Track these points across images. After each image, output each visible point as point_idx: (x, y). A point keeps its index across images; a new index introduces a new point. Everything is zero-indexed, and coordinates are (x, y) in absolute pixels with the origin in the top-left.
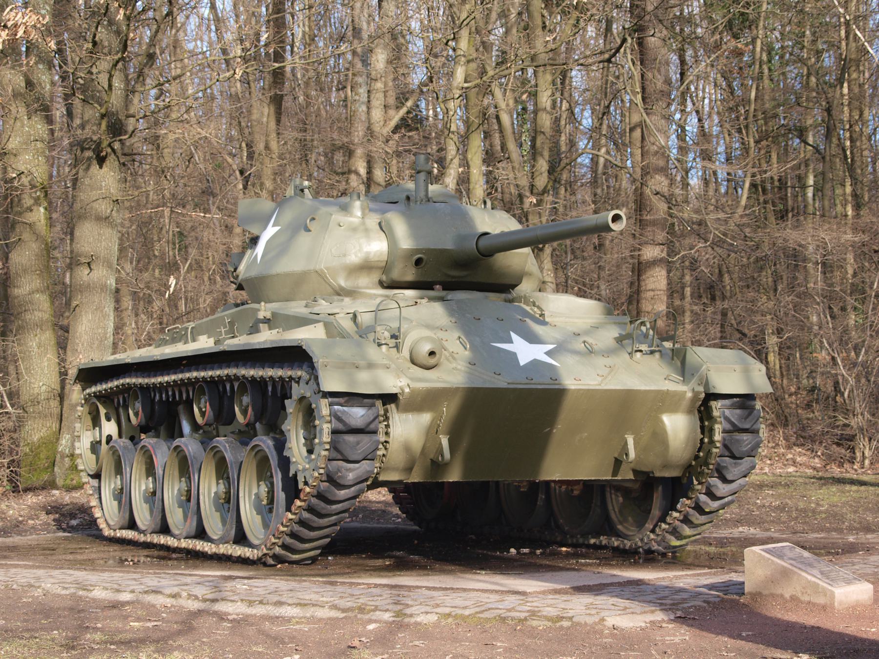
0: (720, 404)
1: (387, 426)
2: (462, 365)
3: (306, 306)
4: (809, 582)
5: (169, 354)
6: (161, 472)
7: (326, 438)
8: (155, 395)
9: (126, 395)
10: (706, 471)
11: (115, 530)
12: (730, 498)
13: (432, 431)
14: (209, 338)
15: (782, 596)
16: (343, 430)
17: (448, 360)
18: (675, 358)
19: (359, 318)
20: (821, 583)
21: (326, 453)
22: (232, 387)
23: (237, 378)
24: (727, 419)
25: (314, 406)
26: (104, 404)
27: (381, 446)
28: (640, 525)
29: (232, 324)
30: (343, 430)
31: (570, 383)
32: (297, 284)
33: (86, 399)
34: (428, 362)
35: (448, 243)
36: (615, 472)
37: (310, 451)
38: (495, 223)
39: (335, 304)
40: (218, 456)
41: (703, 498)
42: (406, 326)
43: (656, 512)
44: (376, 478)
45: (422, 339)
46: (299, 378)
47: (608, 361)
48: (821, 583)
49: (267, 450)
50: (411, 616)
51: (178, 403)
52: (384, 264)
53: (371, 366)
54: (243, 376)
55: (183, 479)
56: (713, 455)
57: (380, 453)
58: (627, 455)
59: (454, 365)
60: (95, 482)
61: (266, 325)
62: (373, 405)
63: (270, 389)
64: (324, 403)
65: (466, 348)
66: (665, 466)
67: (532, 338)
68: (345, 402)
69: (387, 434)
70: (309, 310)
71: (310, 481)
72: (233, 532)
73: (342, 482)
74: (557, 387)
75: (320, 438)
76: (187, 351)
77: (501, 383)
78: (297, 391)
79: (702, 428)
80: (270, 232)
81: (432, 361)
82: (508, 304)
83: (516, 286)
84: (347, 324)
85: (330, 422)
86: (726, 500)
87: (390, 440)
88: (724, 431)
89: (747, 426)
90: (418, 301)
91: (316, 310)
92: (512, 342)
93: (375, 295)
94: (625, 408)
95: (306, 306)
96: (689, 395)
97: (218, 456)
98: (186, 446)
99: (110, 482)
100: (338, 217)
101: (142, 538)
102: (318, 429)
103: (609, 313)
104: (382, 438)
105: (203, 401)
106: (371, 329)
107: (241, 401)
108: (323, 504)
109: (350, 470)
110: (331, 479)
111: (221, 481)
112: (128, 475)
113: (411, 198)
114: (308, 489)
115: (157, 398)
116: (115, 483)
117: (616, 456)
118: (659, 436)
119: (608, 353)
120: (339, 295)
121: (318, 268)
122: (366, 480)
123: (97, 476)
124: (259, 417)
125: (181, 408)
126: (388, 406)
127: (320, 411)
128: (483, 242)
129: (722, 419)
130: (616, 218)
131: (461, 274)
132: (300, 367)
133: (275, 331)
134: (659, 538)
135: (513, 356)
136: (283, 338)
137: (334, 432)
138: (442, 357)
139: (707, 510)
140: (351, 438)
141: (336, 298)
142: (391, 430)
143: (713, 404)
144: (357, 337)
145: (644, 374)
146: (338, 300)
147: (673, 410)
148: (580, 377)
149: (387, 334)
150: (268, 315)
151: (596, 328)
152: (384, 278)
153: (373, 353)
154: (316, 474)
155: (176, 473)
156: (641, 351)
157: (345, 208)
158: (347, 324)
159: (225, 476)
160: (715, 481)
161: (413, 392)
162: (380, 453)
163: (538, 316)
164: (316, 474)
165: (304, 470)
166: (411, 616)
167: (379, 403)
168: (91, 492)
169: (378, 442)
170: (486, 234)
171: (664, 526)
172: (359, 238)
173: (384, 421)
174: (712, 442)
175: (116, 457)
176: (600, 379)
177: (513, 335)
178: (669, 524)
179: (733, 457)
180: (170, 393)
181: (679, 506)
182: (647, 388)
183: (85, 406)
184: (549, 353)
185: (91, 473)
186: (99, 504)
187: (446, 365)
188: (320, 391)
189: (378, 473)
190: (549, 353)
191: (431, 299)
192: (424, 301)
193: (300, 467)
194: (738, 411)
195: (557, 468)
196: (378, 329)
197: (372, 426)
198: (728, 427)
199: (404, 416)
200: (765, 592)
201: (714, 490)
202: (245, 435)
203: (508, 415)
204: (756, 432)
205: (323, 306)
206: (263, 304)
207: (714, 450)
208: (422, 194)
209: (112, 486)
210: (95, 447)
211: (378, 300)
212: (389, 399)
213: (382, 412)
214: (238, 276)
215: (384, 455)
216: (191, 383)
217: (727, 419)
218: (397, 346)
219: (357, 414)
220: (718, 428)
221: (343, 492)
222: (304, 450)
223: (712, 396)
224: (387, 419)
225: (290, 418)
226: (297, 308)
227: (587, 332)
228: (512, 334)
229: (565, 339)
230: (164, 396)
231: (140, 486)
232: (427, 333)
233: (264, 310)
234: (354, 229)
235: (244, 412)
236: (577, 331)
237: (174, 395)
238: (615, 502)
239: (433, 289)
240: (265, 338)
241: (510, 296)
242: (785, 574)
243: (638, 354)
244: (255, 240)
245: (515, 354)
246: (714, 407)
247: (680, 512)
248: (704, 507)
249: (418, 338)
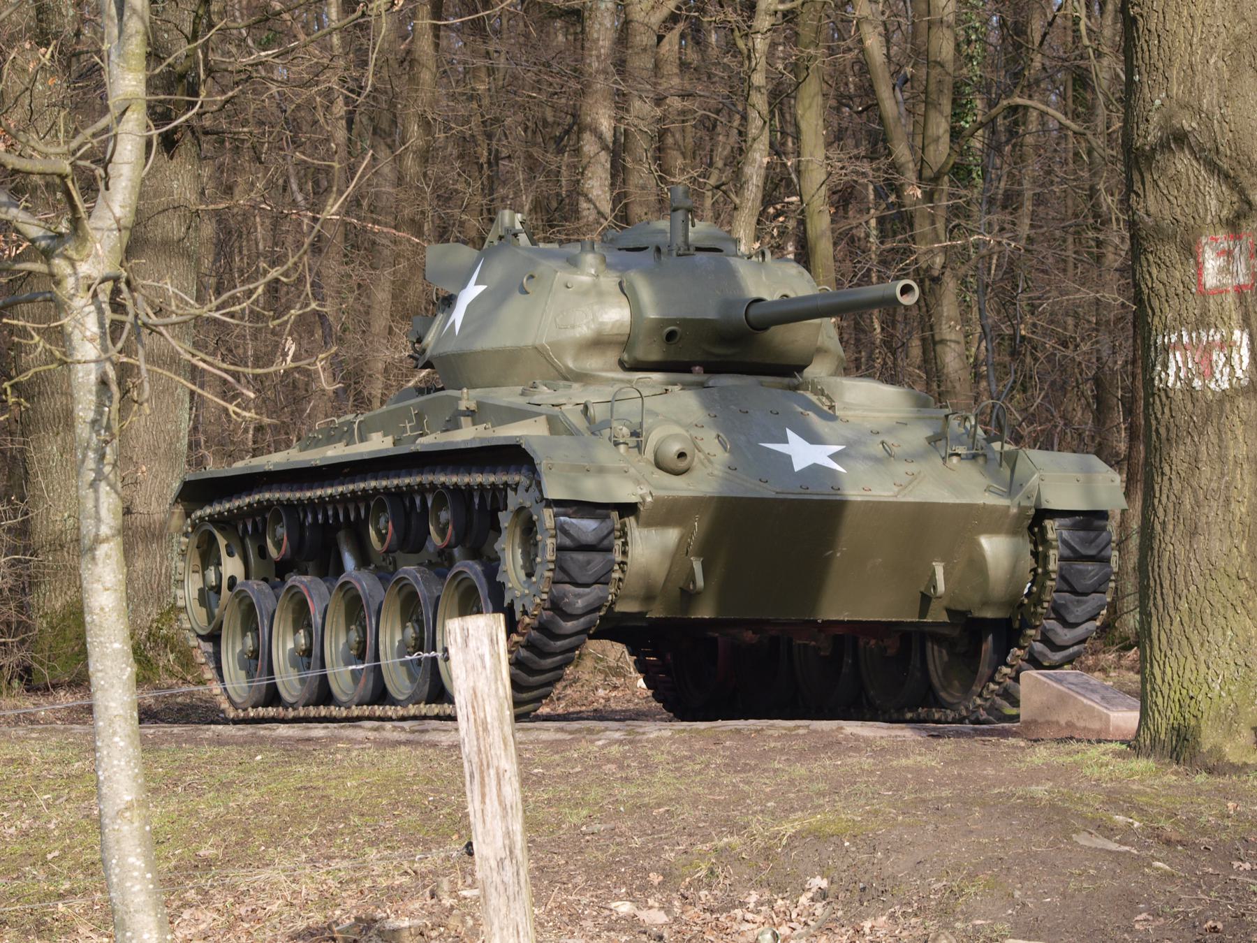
0: (1057, 524)
1: (625, 544)
2: (718, 470)
3: (523, 394)
4: (1085, 705)
5: (332, 458)
6: (319, 621)
7: (550, 556)
8: (306, 516)
9: (258, 519)
10: (1040, 610)
11: (245, 710)
12: (1076, 648)
13: (682, 550)
14: (385, 435)
15: (1058, 723)
16: (572, 546)
17: (703, 464)
18: (1004, 463)
19: (591, 410)
20: (1097, 706)
21: (550, 574)
22: (424, 502)
23: (433, 486)
24: (1064, 542)
25: (535, 517)
26: (221, 530)
27: (616, 567)
28: (967, 690)
29: (419, 416)
30: (572, 546)
31: (853, 493)
32: (509, 364)
33: (194, 526)
34: (675, 466)
35: (709, 311)
36: (923, 612)
37: (529, 575)
38: (773, 281)
39: (560, 392)
40: (405, 591)
41: (1038, 646)
42: (650, 421)
43: (984, 670)
44: (610, 608)
45: (670, 436)
46: (517, 484)
47: (912, 468)
48: (1097, 706)
49: (474, 577)
50: (644, 733)
51: (337, 527)
52: (625, 338)
53: (601, 470)
54: (443, 484)
55: (353, 627)
56: (1048, 589)
57: (616, 575)
58: (935, 588)
59: (710, 470)
60: (208, 647)
61: (469, 419)
62: (608, 517)
63: (477, 501)
64: (548, 513)
65: (725, 449)
66: (985, 604)
67: (813, 438)
68: (575, 512)
69: (625, 553)
70: (527, 399)
71: (530, 609)
72: (426, 688)
73: (569, 610)
74: (838, 498)
75: (544, 556)
76: (362, 454)
77: (768, 492)
78: (513, 500)
79: (1035, 554)
80: (472, 291)
81: (682, 464)
82: (788, 392)
83: (805, 367)
84: (576, 420)
85: (555, 536)
86: (1071, 650)
87: (629, 561)
88: (1062, 559)
89: (1092, 552)
90: (670, 388)
91: (536, 399)
92: (786, 442)
93: (613, 379)
94: (921, 526)
95: (523, 394)
96: (1014, 510)
97: (405, 591)
98: (359, 581)
99: (234, 643)
100: (562, 276)
101: (291, 713)
102: (540, 545)
103: (921, 404)
104: (619, 558)
105: (382, 520)
106: (607, 424)
107: (438, 518)
108: (545, 639)
109: (579, 596)
110: (556, 606)
111: (409, 624)
112: (266, 630)
113: (664, 250)
114: (527, 620)
115: (310, 519)
116: (243, 644)
117: (922, 589)
118: (977, 563)
119: (909, 458)
120: (566, 379)
121: (537, 343)
122: (598, 609)
123: (214, 637)
124: (460, 540)
125: (341, 536)
126: (626, 519)
127: (543, 523)
128: (755, 311)
129: (1059, 543)
130: (906, 290)
131: (727, 352)
132: (518, 471)
133: (481, 427)
134: (988, 704)
135: (787, 459)
136: (496, 435)
137: (560, 549)
138: (696, 459)
139: (1046, 664)
140: (580, 557)
141: (562, 383)
142: (629, 548)
143: (1048, 523)
144: (587, 435)
145: (956, 485)
146: (566, 387)
147: (993, 530)
148: (866, 486)
149: (626, 431)
150: (473, 406)
151: (903, 424)
152: (626, 357)
153: (604, 454)
154: (538, 601)
155: (342, 621)
156: (957, 455)
157: (573, 263)
158: (576, 420)
160: (1051, 624)
161: (657, 501)
162: (616, 575)
163: (826, 408)
164: (538, 601)
165: (524, 596)
166: (644, 733)
167: (615, 515)
168: (203, 660)
169: (613, 562)
170: (759, 300)
171: (992, 686)
172: (590, 302)
173: (620, 537)
174: (1047, 573)
175: (243, 607)
176: (896, 489)
177: (790, 433)
178: (999, 684)
179: (1074, 592)
180: (330, 513)
181: (1009, 658)
182: (958, 501)
183: (192, 536)
184: (833, 457)
185: (202, 633)
186: (216, 676)
187: (699, 472)
188: (543, 499)
189: (613, 603)
190: (833, 457)
191: (686, 386)
192: (676, 388)
193: (518, 594)
194: (1081, 533)
195: (842, 603)
196: (615, 424)
197: (606, 542)
198: (1067, 552)
199: (645, 531)
200: (1041, 720)
201: (1050, 635)
202: (441, 564)
203: (775, 535)
204: (1107, 560)
205: (545, 395)
206: (465, 390)
207: (1049, 583)
208: (679, 240)
209: (238, 649)
210: (208, 596)
211: (616, 387)
212: (628, 509)
213: (618, 526)
214: (424, 351)
215: (620, 580)
216: (366, 495)
217: (1064, 542)
218: (639, 447)
219: (587, 527)
220: (1053, 554)
221: (569, 624)
222: (522, 574)
223: (1042, 514)
224: (624, 535)
225: (504, 533)
226: (507, 396)
227: (890, 431)
228: (788, 431)
229: (858, 439)
230: (320, 517)
231: (285, 644)
232: (677, 430)
233: (467, 399)
234: (585, 293)
235: (442, 532)
236: (876, 428)
237: (336, 515)
238: (937, 658)
239: (690, 372)
240: (467, 435)
241: (795, 381)
242: (1063, 699)
243: (955, 459)
244: (448, 302)
245: (789, 457)
246: (1049, 527)
247: (1012, 666)
248: (1040, 659)
249: (666, 435)
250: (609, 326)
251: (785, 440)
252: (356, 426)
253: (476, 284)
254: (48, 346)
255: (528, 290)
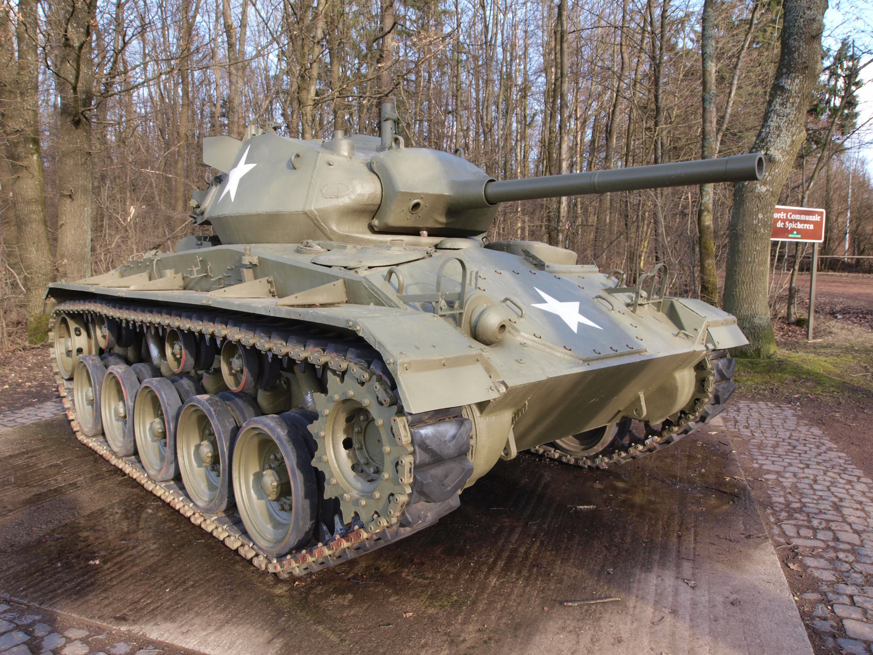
14: (176, 273)
80: (242, 169)
121: (307, 209)
150: (255, 261)
159: (207, 432)
168: (65, 394)
214: (202, 213)
250: (366, 197)
251: (580, 325)
252: (155, 262)
253: (246, 163)
254: (817, 248)
255: (296, 166)
